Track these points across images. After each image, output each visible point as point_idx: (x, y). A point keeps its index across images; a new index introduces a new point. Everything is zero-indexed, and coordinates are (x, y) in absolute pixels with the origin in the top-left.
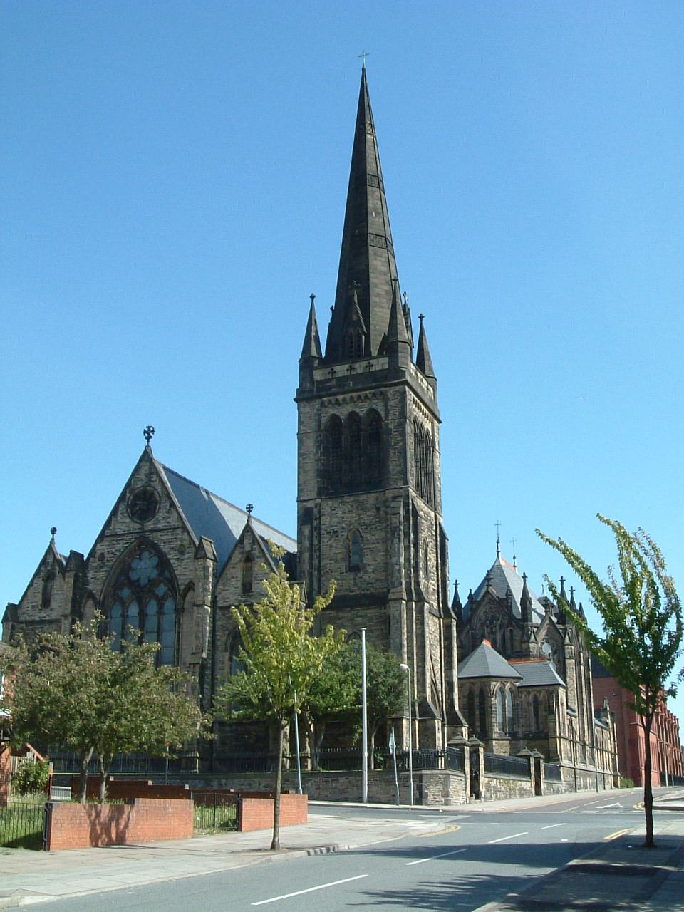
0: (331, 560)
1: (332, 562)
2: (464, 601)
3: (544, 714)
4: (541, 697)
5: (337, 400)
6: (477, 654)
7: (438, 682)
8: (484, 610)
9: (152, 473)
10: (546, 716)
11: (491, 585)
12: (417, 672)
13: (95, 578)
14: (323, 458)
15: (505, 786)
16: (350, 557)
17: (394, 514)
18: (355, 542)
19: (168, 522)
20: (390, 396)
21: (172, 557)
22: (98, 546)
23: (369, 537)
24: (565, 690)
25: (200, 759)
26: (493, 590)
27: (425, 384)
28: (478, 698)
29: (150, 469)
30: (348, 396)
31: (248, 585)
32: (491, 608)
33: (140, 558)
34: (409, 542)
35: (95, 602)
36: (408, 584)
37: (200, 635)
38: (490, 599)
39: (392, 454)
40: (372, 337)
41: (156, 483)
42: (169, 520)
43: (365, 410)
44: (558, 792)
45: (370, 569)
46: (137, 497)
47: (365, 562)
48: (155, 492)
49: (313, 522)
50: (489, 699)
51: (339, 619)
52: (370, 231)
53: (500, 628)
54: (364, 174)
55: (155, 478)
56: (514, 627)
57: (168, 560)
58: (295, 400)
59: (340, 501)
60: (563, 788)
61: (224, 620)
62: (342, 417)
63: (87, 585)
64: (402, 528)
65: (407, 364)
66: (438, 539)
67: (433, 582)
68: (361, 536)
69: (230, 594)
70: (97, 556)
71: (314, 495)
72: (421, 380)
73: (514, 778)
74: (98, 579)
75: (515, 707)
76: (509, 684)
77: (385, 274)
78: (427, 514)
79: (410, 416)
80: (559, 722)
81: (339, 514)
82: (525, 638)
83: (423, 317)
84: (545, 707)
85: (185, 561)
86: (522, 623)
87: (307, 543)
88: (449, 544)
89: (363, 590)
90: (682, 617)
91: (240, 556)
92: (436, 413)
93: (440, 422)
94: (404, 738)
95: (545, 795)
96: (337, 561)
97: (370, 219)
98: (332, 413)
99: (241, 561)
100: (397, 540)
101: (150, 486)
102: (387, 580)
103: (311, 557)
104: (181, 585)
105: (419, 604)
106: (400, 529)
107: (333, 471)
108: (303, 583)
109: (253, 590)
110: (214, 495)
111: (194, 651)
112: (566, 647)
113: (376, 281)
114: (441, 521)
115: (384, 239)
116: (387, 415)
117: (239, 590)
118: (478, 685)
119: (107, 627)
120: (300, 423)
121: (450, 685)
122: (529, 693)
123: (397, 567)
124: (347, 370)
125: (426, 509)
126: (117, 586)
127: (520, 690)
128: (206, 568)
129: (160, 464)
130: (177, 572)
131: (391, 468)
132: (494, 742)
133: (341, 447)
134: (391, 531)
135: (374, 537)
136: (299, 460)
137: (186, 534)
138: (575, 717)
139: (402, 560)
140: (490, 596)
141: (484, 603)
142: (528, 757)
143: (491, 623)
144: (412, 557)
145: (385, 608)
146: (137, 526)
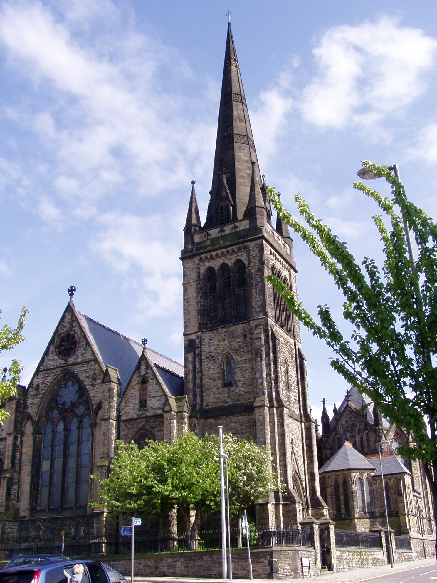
0: (210, 379)
1: (211, 380)
2: (331, 415)
3: (395, 496)
4: (391, 483)
5: (212, 256)
6: (340, 454)
7: (302, 473)
8: (346, 419)
9: (73, 321)
12: (280, 465)
13: (32, 403)
15: (358, 557)
16: (224, 376)
17: (256, 339)
19: (85, 357)
20: (251, 249)
21: (87, 383)
22: (35, 380)
23: (239, 359)
24: (410, 477)
25: (107, 544)
26: (353, 405)
27: (282, 242)
28: (342, 487)
29: (72, 318)
30: (219, 252)
31: (144, 402)
32: (351, 418)
33: (65, 386)
35: (32, 422)
36: (270, 394)
37: (106, 442)
39: (254, 293)
40: (238, 207)
41: (76, 328)
42: (85, 355)
43: (233, 261)
44: (409, 559)
46: (63, 340)
47: (236, 379)
48: (76, 335)
49: (195, 350)
50: (350, 487)
52: (235, 132)
53: (359, 433)
54: (230, 93)
55: (75, 324)
56: (369, 432)
57: (85, 386)
58: (181, 259)
59: (215, 332)
60: (414, 555)
61: (126, 430)
62: (216, 268)
63: (27, 409)
64: (263, 349)
65: (264, 224)
66: (298, 360)
67: (295, 394)
68: (233, 359)
70: (34, 386)
71: (196, 329)
72: (278, 238)
73: (366, 550)
74: (35, 404)
75: (371, 493)
76: (366, 474)
77: (247, 162)
78: (286, 343)
79: (268, 263)
80: (407, 502)
81: (216, 343)
82: (378, 439)
83: (280, 195)
84: (395, 491)
85: (97, 386)
86: (374, 428)
87: (191, 367)
88: (307, 364)
89: (235, 401)
91: (138, 379)
92: (293, 265)
93: (296, 272)
94: (270, 520)
95: (397, 562)
96: (214, 380)
97: (235, 124)
98: (208, 266)
99: (138, 383)
100: (260, 359)
101: (72, 330)
102: (253, 391)
103: (195, 378)
104: (94, 405)
105: (280, 409)
106: (262, 350)
107: (211, 311)
108: (185, 397)
109: (147, 405)
110: (132, 341)
111: (102, 456)
113: (240, 167)
114: (300, 346)
115: (246, 138)
116: (249, 263)
117: (137, 406)
118: (342, 476)
119: (41, 441)
121: (312, 475)
123: (260, 381)
124: (219, 232)
125: (286, 336)
126: (49, 409)
127: (375, 478)
128: (110, 390)
129: (82, 315)
130: (91, 395)
131: (253, 304)
132: (356, 520)
133: (216, 292)
134: (255, 352)
135: (242, 359)
137: (97, 365)
138: (421, 498)
139: (264, 374)
140: (350, 409)
141: (345, 414)
142: (379, 532)
143: (352, 429)
144: (272, 372)
145: (253, 415)
146: (62, 362)
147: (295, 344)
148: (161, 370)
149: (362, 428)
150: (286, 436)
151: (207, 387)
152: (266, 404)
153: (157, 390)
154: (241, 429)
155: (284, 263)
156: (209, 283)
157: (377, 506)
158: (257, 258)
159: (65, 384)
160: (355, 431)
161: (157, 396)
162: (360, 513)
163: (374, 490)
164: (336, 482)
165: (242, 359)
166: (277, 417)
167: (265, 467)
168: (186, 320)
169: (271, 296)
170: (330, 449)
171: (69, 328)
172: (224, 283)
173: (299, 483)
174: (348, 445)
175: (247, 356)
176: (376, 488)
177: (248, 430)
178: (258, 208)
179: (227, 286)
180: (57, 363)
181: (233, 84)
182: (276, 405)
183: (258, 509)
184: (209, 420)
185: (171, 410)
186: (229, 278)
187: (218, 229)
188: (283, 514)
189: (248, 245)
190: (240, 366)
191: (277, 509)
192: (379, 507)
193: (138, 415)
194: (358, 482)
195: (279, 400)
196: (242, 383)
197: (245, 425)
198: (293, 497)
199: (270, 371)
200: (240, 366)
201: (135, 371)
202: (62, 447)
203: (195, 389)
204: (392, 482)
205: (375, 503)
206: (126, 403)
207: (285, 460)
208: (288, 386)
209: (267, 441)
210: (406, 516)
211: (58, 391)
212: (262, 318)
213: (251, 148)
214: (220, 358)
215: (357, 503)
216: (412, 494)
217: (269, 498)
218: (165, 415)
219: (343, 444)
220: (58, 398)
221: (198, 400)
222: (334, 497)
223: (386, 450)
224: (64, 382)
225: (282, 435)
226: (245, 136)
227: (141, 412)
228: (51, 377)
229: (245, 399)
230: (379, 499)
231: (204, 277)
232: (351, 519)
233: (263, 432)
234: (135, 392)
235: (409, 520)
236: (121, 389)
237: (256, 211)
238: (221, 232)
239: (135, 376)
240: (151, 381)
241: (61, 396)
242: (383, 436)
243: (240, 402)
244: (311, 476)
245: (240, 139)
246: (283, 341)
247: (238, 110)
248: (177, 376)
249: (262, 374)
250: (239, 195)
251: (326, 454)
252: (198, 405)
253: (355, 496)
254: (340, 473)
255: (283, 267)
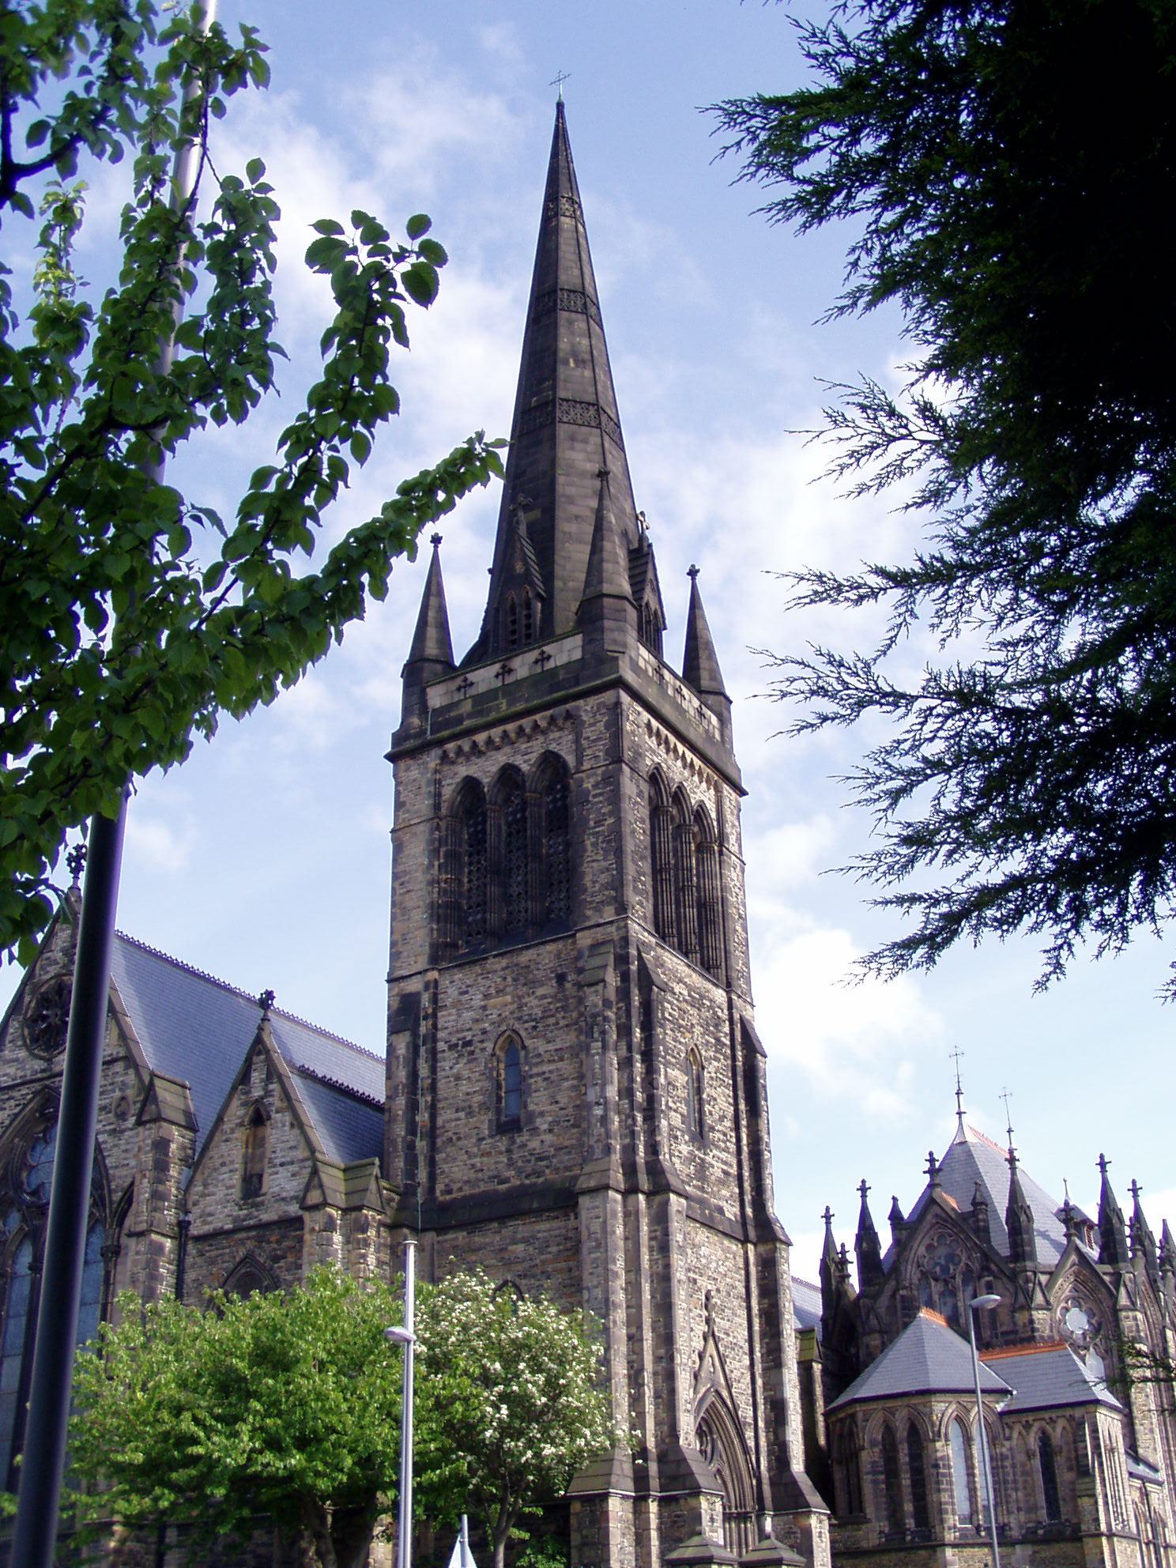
0: (457, 1111)
1: (462, 1115)
5: (475, 744)
8: (926, 1241)
10: (1073, 1483)
11: (939, 1185)
12: (655, 1374)
14: (444, 877)
16: (499, 1099)
17: (590, 985)
18: (513, 1063)
20: (585, 718)
30: (496, 733)
31: (255, 1180)
34: (630, 1048)
36: (630, 1150)
38: (937, 1216)
39: (589, 848)
43: (534, 757)
45: (542, 1124)
47: (531, 1107)
50: (930, 1445)
51: (474, 1251)
52: (562, 394)
53: (965, 1283)
54: (554, 291)
58: (390, 757)
59: (477, 969)
62: (485, 780)
65: (625, 645)
67: (724, 1156)
68: (524, 1047)
69: (217, 1203)
71: (422, 963)
72: (678, 691)
78: (698, 1000)
80: (1106, 1496)
81: (478, 1001)
82: (1021, 1299)
84: (1069, 1459)
87: (402, 1074)
89: (527, 1177)
90: (265, 48)
91: (241, 1112)
92: (731, 772)
94: (614, 1550)
96: (470, 1114)
97: (562, 371)
99: (241, 1124)
103: (413, 1107)
104: (116, 1191)
105: (658, 1199)
107: (470, 907)
109: (264, 1190)
112: (1124, 1314)
113: (571, 491)
114: (748, 1013)
115: (592, 411)
116: (579, 761)
117: (236, 1193)
118: (904, 1412)
120: (399, 805)
121: (777, 1408)
122: (1027, 1426)
123: (598, 1111)
124: (497, 676)
125: (696, 979)
127: (1007, 1419)
128: (162, 1145)
131: (587, 881)
132: (949, 1552)
135: (551, 1047)
136: (393, 889)
137: (131, 1071)
138: (1160, 1484)
139: (612, 1092)
140: (939, 1211)
141: (926, 1225)
143: (945, 1269)
146: (39, 1065)
147: (730, 1006)
148: (319, 1087)
149: (976, 1266)
150: (675, 1282)
151: (450, 1134)
152: (612, 1183)
153: (292, 1144)
154: (543, 1262)
155: (697, 763)
156: (469, 826)
157: (1013, 1506)
158: (600, 745)
159: (45, 1132)
160: (954, 1277)
161: (292, 1163)
162: (960, 1530)
163: (1003, 1457)
164: (889, 1430)
165: (551, 1047)
166: (650, 1225)
167: (570, 1374)
168: (397, 937)
169: (642, 858)
170: (881, 1332)
171: (64, 966)
172: (509, 825)
173: (733, 1433)
174: (930, 1319)
175: (567, 1039)
176: (1011, 1449)
177: (563, 1265)
178: (611, 600)
179: (518, 832)
180: (23, 1069)
181: (563, 263)
182: (645, 1185)
183: (577, 1514)
184: (449, 1236)
185: (325, 1204)
186: (523, 811)
187: (497, 667)
188: (659, 1529)
189: (578, 708)
190: (545, 1068)
191: (641, 1513)
192: (1019, 1509)
193: (236, 1219)
194: (954, 1430)
195: (655, 1169)
196: (550, 1119)
197: (554, 1249)
198: (692, 1474)
199: (631, 1080)
200: (545, 1068)
201: (234, 1089)
202: (24, 1320)
203: (414, 1142)
204: (1059, 1430)
205: (1008, 1496)
206: (205, 1185)
207: (671, 1358)
208: (700, 1134)
209: (612, 1298)
210: (1104, 1540)
211: (25, 1154)
212: (612, 922)
213: (606, 438)
214: (489, 1045)
215: (952, 1497)
216: (1124, 1468)
217: (614, 1479)
218: (307, 1216)
219: (914, 1316)
220: (24, 1174)
221: (422, 1175)
222: (882, 1477)
223: (1047, 1332)
224: (42, 1127)
225: (664, 1279)
226: (589, 404)
227: (245, 1212)
228: (7, 1112)
229: (557, 1170)
230: (1020, 1485)
231: (451, 808)
232: (934, 1548)
233: (600, 1270)
234: (231, 1151)
235: (1113, 1553)
236: (193, 1141)
237: (602, 607)
238: (503, 674)
239: (235, 1103)
240: (279, 1115)
241: (33, 1168)
242: (1038, 1289)
243: (541, 1180)
244: (773, 1408)
245: (575, 413)
246: (686, 993)
247: (573, 334)
248: (365, 1101)
249: (603, 1090)
250: (564, 569)
251: (868, 1346)
252: (419, 1190)
253: (944, 1475)
254: (898, 1403)
255: (696, 778)
